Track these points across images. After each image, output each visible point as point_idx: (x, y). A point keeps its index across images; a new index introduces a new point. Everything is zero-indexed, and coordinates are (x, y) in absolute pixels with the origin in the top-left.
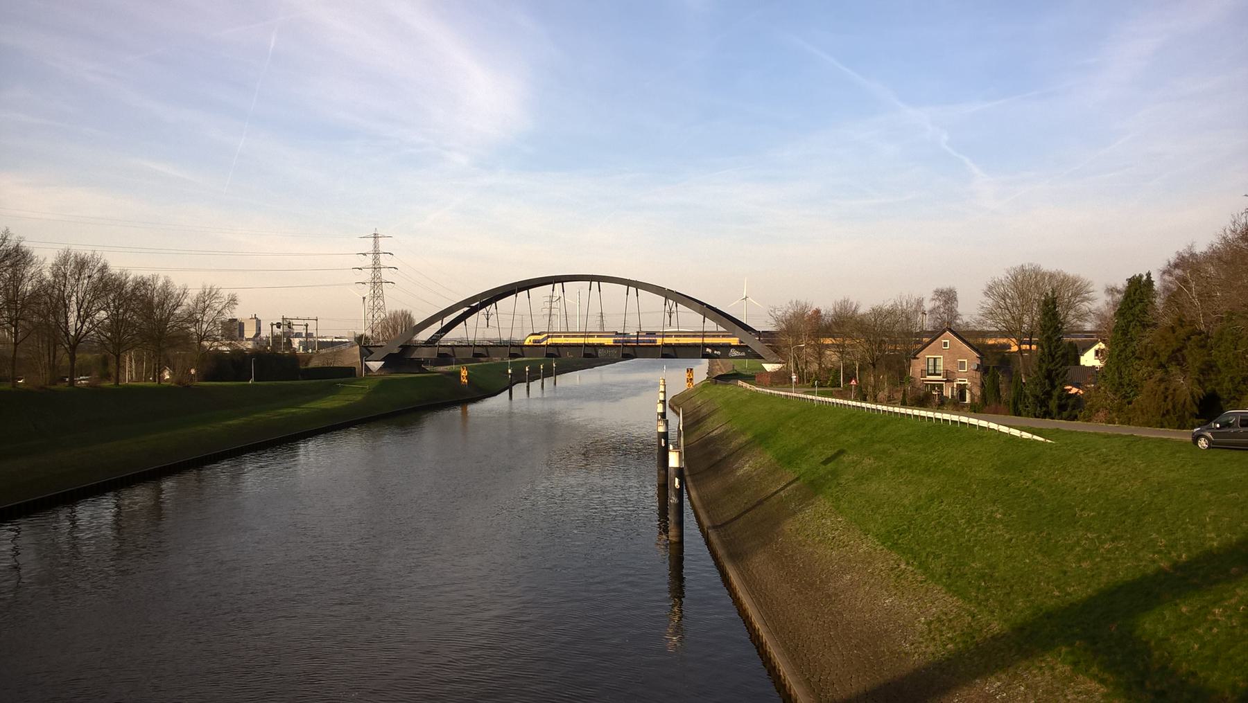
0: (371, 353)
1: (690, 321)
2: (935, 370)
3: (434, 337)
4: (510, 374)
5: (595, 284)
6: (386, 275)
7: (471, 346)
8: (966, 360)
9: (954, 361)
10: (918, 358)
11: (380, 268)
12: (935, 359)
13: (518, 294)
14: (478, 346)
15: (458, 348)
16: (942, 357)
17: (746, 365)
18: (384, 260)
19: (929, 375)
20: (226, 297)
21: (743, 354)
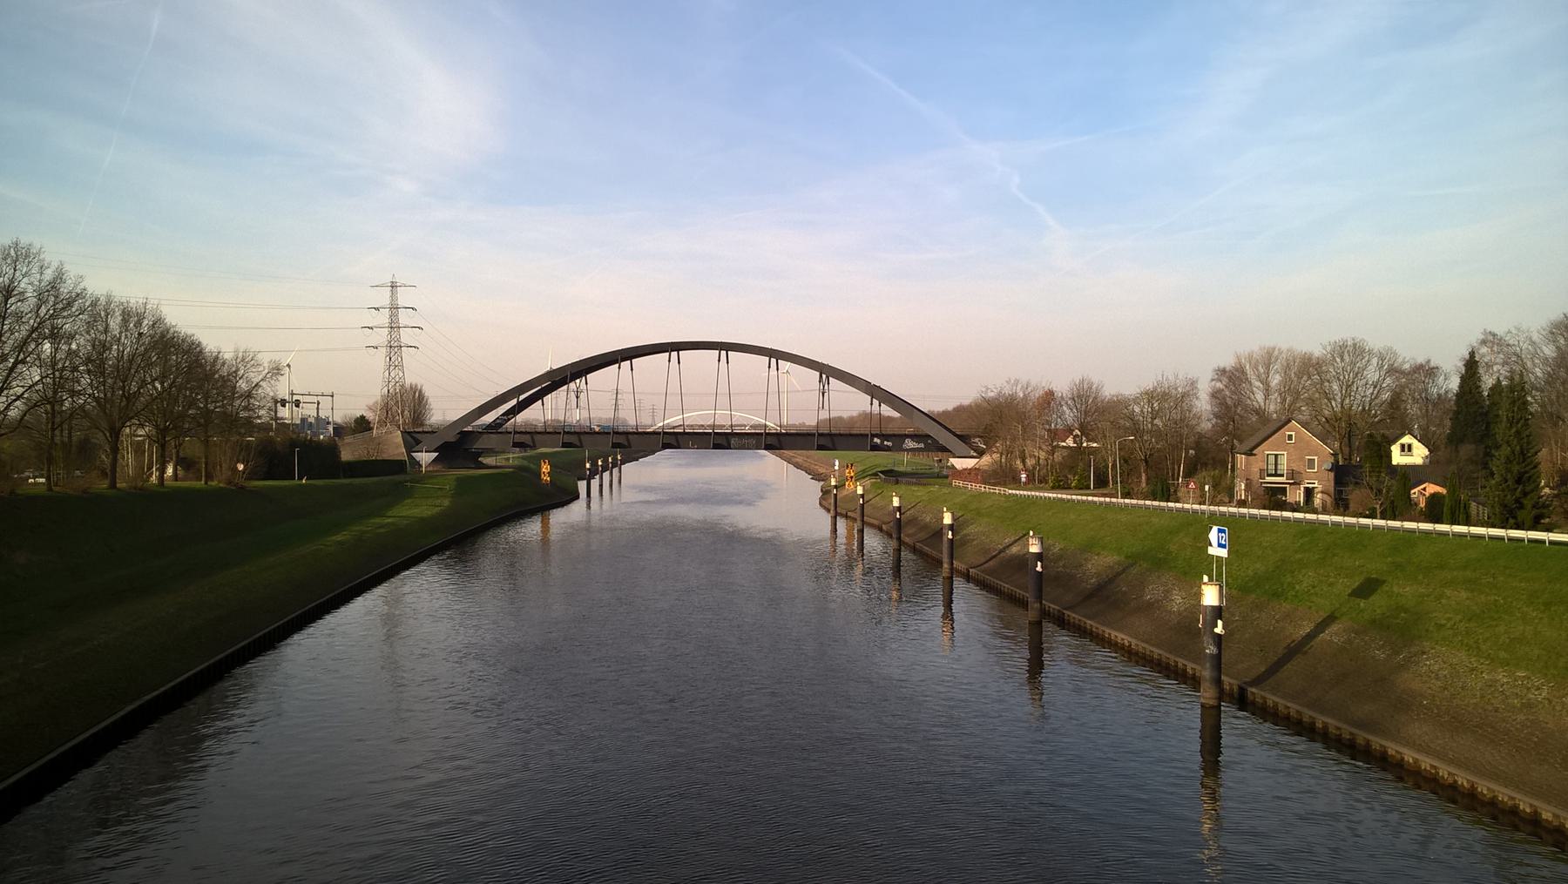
0: (418, 442)
1: (849, 404)
2: (1276, 470)
3: (498, 421)
4: (589, 469)
5: (674, 354)
6: (406, 336)
7: (510, 433)
8: (1316, 458)
9: (1302, 459)
10: (1255, 455)
11: (399, 327)
12: (1276, 456)
13: (622, 364)
14: (568, 433)
15: (540, 435)
16: (1285, 453)
17: (928, 461)
18: (404, 318)
19: (1269, 475)
20: (266, 365)
21: (922, 445)
